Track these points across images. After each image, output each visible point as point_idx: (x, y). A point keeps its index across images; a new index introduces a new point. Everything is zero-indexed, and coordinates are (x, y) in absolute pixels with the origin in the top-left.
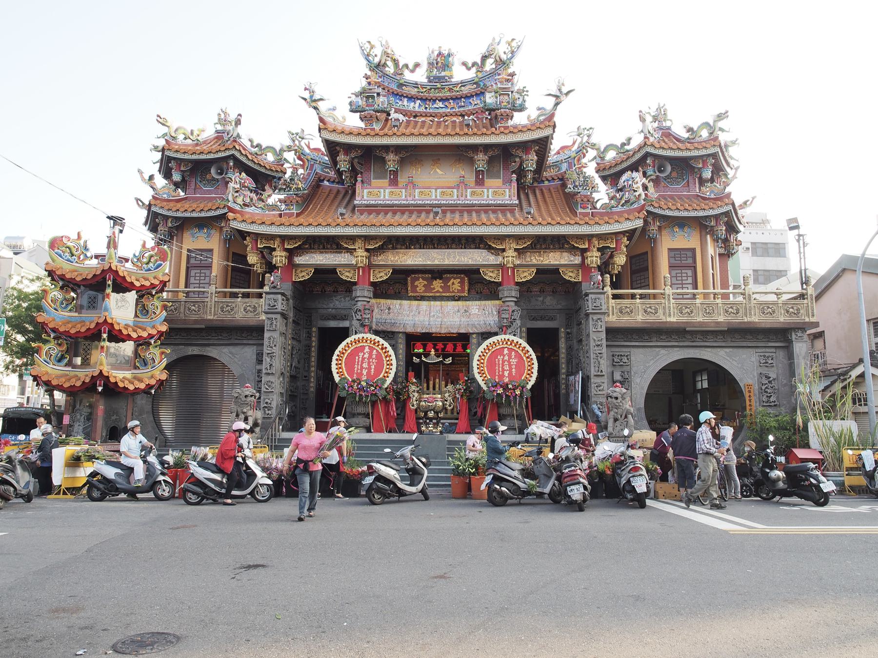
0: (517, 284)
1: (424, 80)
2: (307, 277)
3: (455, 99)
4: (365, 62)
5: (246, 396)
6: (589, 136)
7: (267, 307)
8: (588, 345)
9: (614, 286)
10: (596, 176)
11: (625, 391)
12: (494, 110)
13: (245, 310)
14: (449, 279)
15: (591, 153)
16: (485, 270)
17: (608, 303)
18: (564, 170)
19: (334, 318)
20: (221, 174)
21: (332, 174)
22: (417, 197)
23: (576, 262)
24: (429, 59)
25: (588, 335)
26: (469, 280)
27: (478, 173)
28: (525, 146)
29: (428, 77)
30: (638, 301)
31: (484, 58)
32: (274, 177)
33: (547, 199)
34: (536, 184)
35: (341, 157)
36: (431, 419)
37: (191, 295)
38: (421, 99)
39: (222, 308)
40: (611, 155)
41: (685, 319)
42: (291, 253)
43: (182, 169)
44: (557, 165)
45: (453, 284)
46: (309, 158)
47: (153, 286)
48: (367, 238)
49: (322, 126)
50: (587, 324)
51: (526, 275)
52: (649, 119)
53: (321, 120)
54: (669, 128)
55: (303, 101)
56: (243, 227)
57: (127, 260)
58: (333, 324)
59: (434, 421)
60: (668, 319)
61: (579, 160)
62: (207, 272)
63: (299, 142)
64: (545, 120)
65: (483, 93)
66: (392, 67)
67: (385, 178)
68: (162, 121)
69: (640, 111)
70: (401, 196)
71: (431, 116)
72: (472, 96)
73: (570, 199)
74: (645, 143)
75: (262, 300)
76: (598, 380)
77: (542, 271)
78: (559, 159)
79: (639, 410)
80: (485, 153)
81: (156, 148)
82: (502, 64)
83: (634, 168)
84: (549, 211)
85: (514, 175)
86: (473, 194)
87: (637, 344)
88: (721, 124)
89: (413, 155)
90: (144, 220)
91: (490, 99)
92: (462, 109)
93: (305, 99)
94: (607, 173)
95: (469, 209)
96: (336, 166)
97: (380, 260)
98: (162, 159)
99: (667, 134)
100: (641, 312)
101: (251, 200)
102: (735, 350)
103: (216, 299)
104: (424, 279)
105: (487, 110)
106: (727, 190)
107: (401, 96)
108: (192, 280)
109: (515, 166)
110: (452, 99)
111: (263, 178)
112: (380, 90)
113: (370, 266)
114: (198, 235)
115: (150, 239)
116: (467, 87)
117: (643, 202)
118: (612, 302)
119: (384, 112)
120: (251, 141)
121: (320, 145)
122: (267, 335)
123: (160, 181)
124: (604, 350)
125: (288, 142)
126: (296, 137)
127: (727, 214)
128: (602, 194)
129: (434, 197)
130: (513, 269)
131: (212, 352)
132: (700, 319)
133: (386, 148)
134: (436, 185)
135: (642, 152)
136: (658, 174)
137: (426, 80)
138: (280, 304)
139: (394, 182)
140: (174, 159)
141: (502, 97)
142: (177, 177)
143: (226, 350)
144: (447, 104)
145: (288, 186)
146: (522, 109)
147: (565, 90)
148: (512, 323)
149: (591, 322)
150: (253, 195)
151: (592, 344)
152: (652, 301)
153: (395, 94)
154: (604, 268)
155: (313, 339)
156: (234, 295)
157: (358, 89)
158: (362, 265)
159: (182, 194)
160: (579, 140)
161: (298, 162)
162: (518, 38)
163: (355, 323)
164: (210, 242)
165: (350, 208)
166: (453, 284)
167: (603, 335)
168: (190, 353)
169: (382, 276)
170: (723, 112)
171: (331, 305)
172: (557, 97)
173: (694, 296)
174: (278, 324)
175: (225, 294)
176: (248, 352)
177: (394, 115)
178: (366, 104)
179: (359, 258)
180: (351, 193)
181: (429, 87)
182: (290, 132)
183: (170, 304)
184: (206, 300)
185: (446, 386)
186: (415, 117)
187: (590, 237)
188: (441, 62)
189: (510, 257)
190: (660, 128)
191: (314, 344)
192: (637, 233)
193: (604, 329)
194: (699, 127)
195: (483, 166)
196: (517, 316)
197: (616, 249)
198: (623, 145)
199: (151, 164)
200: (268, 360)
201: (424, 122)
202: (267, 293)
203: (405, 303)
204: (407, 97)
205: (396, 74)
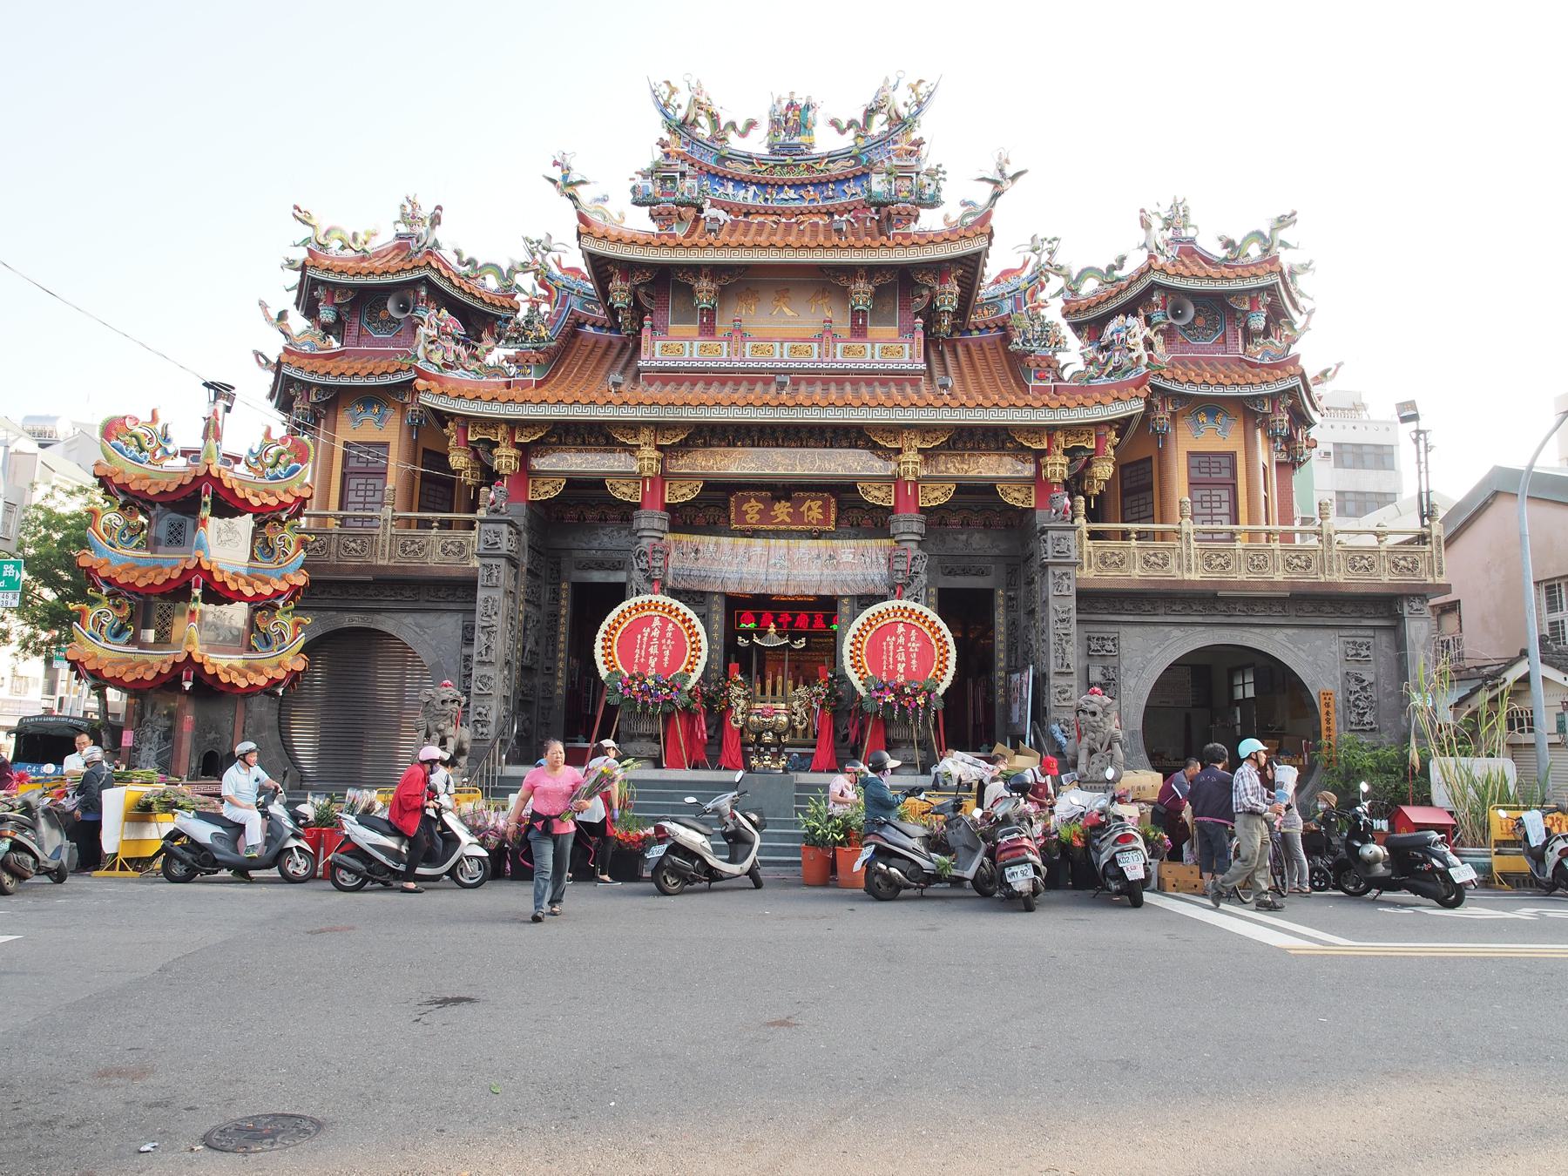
0: (922, 510)
1: (763, 150)
2: (553, 494)
4: (661, 118)
5: (443, 702)
6: (1051, 253)
7: (482, 545)
8: (1045, 619)
9: (1092, 516)
10: (1063, 323)
12: (885, 205)
13: (443, 549)
14: (804, 500)
15: (1055, 283)
17: (1081, 546)
19: (601, 566)
20: (405, 310)
21: (600, 313)
22: (748, 356)
23: (1027, 474)
25: (1046, 602)
26: (838, 502)
27: (855, 314)
28: (939, 269)
29: (771, 146)
30: (1134, 543)
31: (870, 113)
32: (498, 318)
35: (616, 284)
36: (768, 746)
37: (350, 522)
38: (758, 184)
39: (404, 546)
40: (1089, 287)
41: (1215, 576)
42: (526, 451)
43: (337, 300)
44: (994, 302)
45: (810, 508)
46: (560, 284)
47: (283, 506)
48: (660, 427)
51: (937, 496)
52: (1157, 224)
53: (582, 218)
54: (1192, 241)
56: (442, 404)
57: (237, 460)
58: (598, 577)
60: (1187, 577)
61: (1033, 295)
62: (379, 483)
63: (543, 256)
64: (974, 223)
65: (866, 175)
66: (708, 127)
69: (1142, 211)
70: (721, 354)
72: (847, 180)
76: (1063, 682)
77: (966, 489)
81: (291, 264)
82: (900, 124)
83: (1129, 309)
86: (846, 351)
88: (1283, 235)
89: (741, 281)
91: (878, 185)
92: (829, 203)
93: (554, 182)
95: (839, 377)
96: (606, 300)
97: (682, 465)
99: (1189, 250)
101: (458, 356)
102: (1304, 631)
103: (394, 531)
105: (873, 204)
106: (1293, 350)
107: (723, 178)
108: (352, 497)
109: (920, 303)
110: (812, 184)
111: (478, 319)
112: (685, 168)
113: (664, 477)
116: (839, 164)
117: (1144, 370)
119: (690, 204)
120: (458, 253)
121: (576, 260)
122: (481, 594)
123: (298, 323)
124: (1073, 629)
125: (522, 256)
126: (539, 247)
127: (1292, 392)
128: (1073, 355)
129: (777, 357)
130: (915, 484)
131: (386, 623)
133: (696, 269)
134: (782, 334)
136: (1171, 320)
137: (767, 151)
138: (505, 541)
139: (708, 329)
140: (323, 283)
141: (899, 182)
142: (327, 315)
144: (802, 192)
146: (934, 203)
147: (1010, 172)
150: (461, 349)
151: (1052, 617)
152: (1158, 544)
153: (713, 176)
154: (1075, 485)
155: (563, 602)
156: (425, 524)
157: (647, 165)
159: (336, 345)
160: (1034, 259)
163: (637, 576)
164: (385, 430)
165: (631, 373)
166: (810, 508)
167: (1072, 603)
168: (346, 625)
169: (684, 493)
170: (1288, 213)
171: (595, 544)
172: (996, 183)
173: (1232, 536)
175: (408, 522)
176: (450, 625)
177: (709, 212)
178: (660, 191)
182: (526, 239)
184: (376, 531)
185: (795, 688)
186: (747, 214)
187: (1050, 430)
189: (911, 463)
191: (563, 612)
192: (1134, 425)
193: (1073, 591)
194: (1245, 240)
195: (865, 304)
196: (921, 566)
197: (1096, 451)
198: (1112, 268)
199: (282, 291)
201: (761, 224)
202: (482, 521)
203: (725, 541)
204: (732, 179)
205: (713, 138)
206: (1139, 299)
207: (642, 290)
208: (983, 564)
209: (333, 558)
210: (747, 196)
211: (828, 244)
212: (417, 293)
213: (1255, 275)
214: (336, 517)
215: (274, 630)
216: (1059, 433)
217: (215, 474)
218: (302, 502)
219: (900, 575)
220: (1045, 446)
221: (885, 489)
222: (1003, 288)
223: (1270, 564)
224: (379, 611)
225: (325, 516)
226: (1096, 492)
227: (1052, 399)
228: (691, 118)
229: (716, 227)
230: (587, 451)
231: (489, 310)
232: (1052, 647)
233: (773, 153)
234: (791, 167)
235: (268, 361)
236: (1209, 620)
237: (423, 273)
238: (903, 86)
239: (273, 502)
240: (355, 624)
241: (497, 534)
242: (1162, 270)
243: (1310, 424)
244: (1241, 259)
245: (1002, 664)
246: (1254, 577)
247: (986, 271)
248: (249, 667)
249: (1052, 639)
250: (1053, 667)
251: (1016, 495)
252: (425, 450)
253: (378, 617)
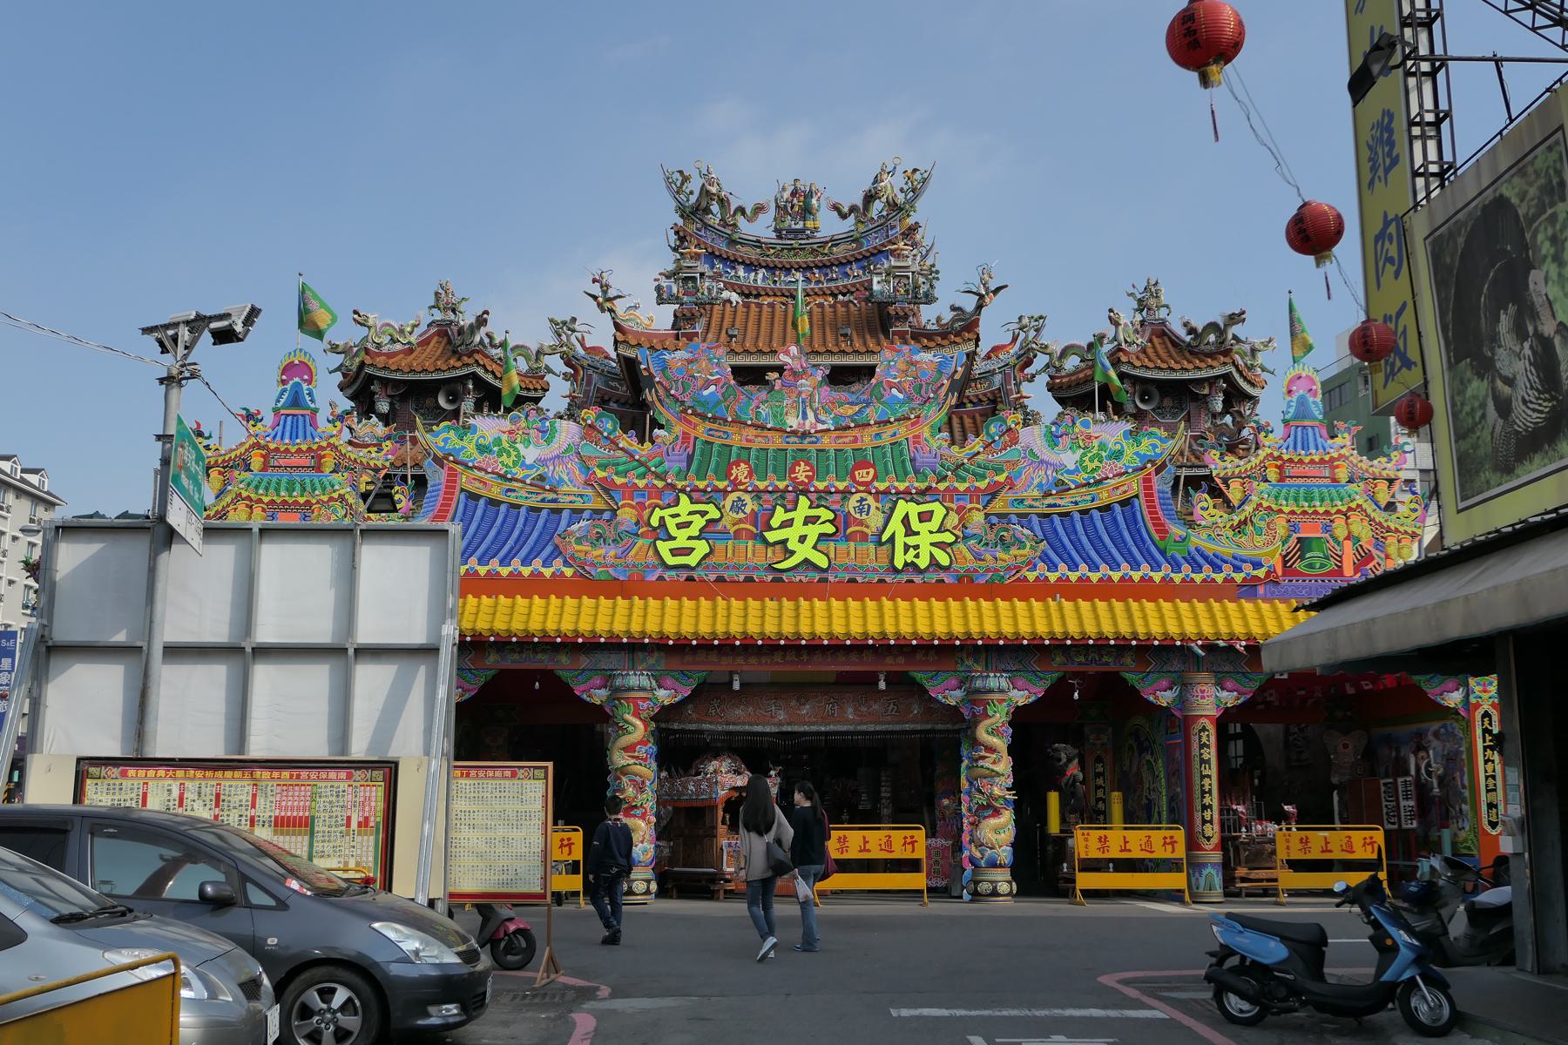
3: (822, 267)
15: (1041, 361)
29: (776, 230)
31: (870, 198)
38: (767, 267)
40: (1072, 362)
49: (620, 337)
53: (617, 326)
69: (1111, 310)
78: (989, 368)
88: (1235, 330)
92: (832, 284)
93: (595, 298)
99: (1161, 332)
107: (732, 262)
116: (842, 247)
125: (549, 340)
126: (563, 327)
146: (929, 299)
153: (724, 260)
160: (1022, 335)
182: (551, 321)
186: (758, 296)
194: (1205, 329)
204: (743, 263)
211: (835, 349)
212: (465, 385)
222: (993, 365)
228: (704, 204)
233: (780, 237)
237: (471, 370)
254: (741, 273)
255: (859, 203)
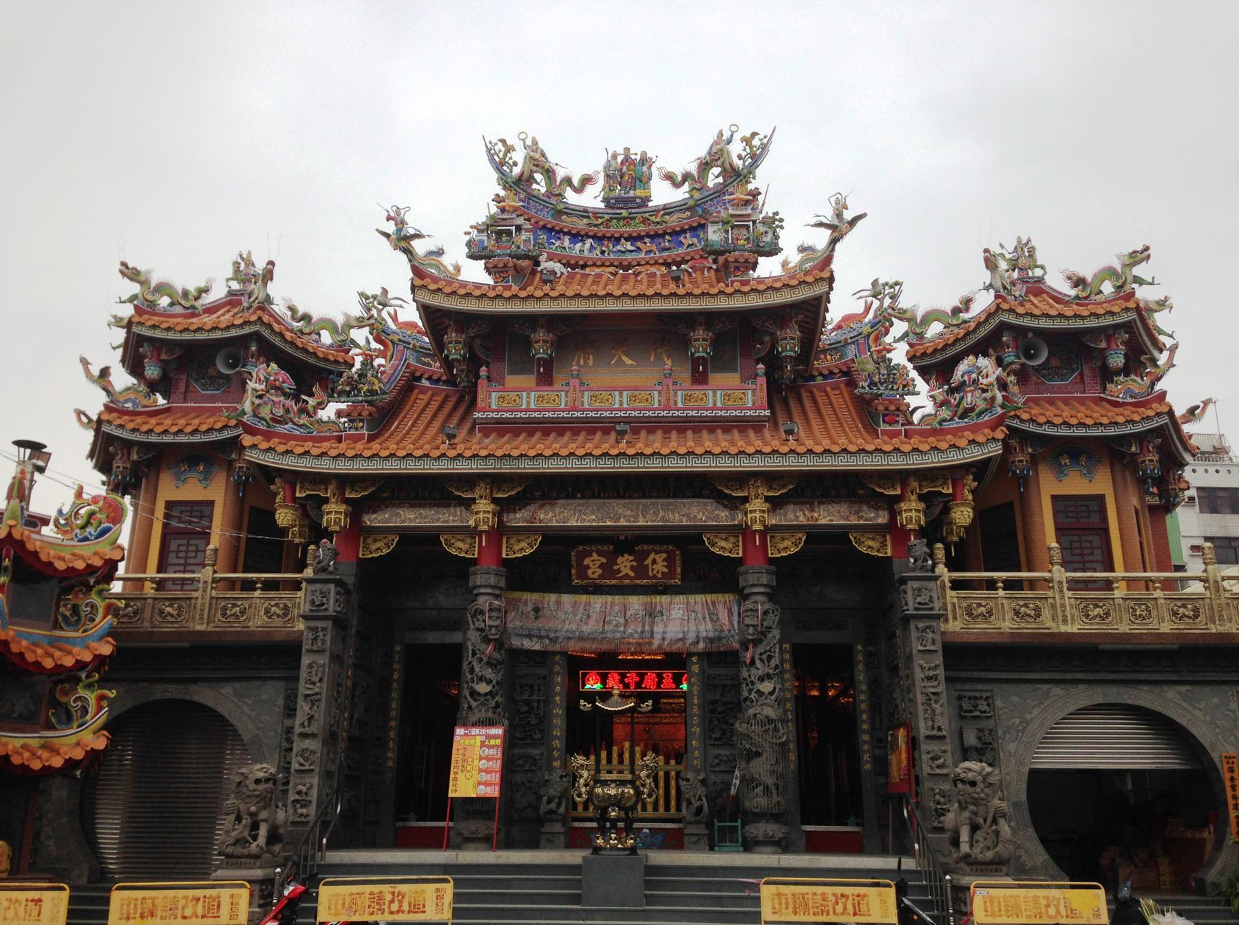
0: (772, 561)
1: (599, 204)
2: (385, 551)
3: (654, 237)
4: (495, 175)
5: (258, 781)
6: (894, 297)
7: (308, 607)
8: (910, 676)
9: (952, 565)
10: (910, 366)
11: (989, 769)
12: (722, 253)
13: (267, 612)
14: (648, 554)
15: (899, 328)
16: (711, 536)
17: (944, 597)
18: (850, 356)
19: (436, 626)
20: (233, 366)
21: (436, 366)
22: (589, 405)
23: (880, 521)
24: (607, 167)
25: (909, 658)
26: (683, 555)
27: (696, 362)
28: (780, 315)
29: (605, 200)
30: (1001, 593)
31: (705, 166)
32: (331, 372)
33: (823, 410)
34: (800, 382)
35: (452, 336)
36: (614, 822)
37: (169, 585)
38: (594, 237)
39: (225, 609)
40: (935, 329)
41: (1094, 628)
42: (357, 509)
43: (164, 356)
44: (837, 348)
45: (654, 562)
46: (395, 338)
47: (91, 569)
48: (495, 480)
49: (418, 282)
50: (906, 636)
51: (787, 547)
52: (1003, 265)
53: (417, 271)
54: (1040, 280)
55: (384, 239)
56: (269, 460)
57: (45, 521)
58: (432, 637)
59: (621, 825)
60: (1064, 629)
61: (877, 339)
62: (201, 543)
63: (379, 311)
64: (813, 268)
65: (702, 227)
66: (543, 183)
67: (531, 373)
68: (129, 273)
70: (557, 401)
71: (612, 265)
72: (683, 231)
73: (875, 408)
74: (998, 307)
75: (299, 594)
76: (935, 747)
77: (817, 537)
79: (1016, 805)
80: (708, 328)
81: (118, 321)
82: (735, 176)
83: (979, 349)
84: (826, 428)
85: (761, 366)
86: (687, 398)
87: (1005, 676)
88: (1137, 271)
89: (582, 334)
90: (88, 448)
91: (714, 234)
92: (666, 254)
93: (387, 235)
94: (929, 361)
95: (682, 426)
96: (442, 352)
97: (518, 519)
98: (127, 339)
99: (1037, 288)
100: (1009, 615)
101: (287, 411)
102: (1197, 689)
103: (214, 593)
104: (600, 554)
105: (710, 253)
106: (1159, 386)
107: (558, 232)
108: (172, 559)
109: (761, 349)
110: (648, 236)
111: (310, 371)
112: (520, 221)
113: (499, 533)
114: (188, 475)
115: (95, 484)
117: (1000, 411)
118: (951, 594)
119: (526, 257)
120: (292, 309)
121: (410, 314)
122: (305, 660)
123: (122, 379)
124: (942, 688)
125: (357, 311)
126: (376, 302)
127: (1160, 431)
128: (922, 400)
129: (617, 406)
130: (763, 534)
131: (204, 695)
132: (1124, 628)
133: (533, 320)
134: (621, 386)
135: (994, 322)
136: (1023, 360)
137: (602, 205)
138: (332, 603)
139: (546, 379)
140: (151, 340)
141: (736, 231)
142: (152, 372)
143: (227, 689)
144: (639, 244)
145: (354, 385)
146: (773, 251)
147: (848, 215)
148: (764, 634)
149: (914, 634)
150: (290, 403)
151: (919, 675)
152: (1029, 594)
153: (549, 230)
154: (933, 530)
155: (396, 666)
156: (249, 585)
157: (482, 218)
158: (485, 528)
159: (161, 401)
160: (876, 304)
161: (374, 345)
162: (764, 131)
163: (473, 636)
164: (215, 491)
165: (467, 426)
166: (654, 562)
167: (939, 659)
168: (157, 697)
169: (523, 548)
170: (1139, 248)
171: (430, 603)
172: (832, 227)
173: (1108, 585)
174: (328, 638)
175: (231, 584)
176: (272, 692)
177: (546, 265)
178: (491, 241)
179: (481, 515)
180: (468, 399)
181: (607, 217)
182: (362, 295)
183: (122, 604)
184: (195, 594)
185: (644, 755)
186: (584, 267)
187: (902, 477)
188: (629, 174)
189: (757, 511)
190: (1024, 281)
191: (396, 676)
192: (993, 468)
193: (938, 647)
195: (705, 350)
196: (772, 620)
197: (953, 496)
198: (956, 311)
199: (107, 349)
200: (306, 708)
201: (599, 276)
202: (309, 581)
203: (567, 599)
204: (569, 233)
205: (550, 194)
206: (991, 337)
207: (478, 342)
208: (837, 602)
209: (146, 624)
210: (583, 249)
212: (247, 348)
213: (953, 446)
214: (152, 580)
215: (74, 706)
216: (912, 478)
217: (17, 536)
218: (112, 565)
219: (751, 630)
220: (899, 492)
221: (732, 539)
223: (1154, 613)
224: (195, 681)
225: (142, 580)
226: (955, 539)
227: (902, 443)
229: (552, 278)
230: (422, 506)
231: (323, 365)
232: (920, 708)
234: (628, 220)
235: (90, 420)
236: (1090, 676)
238: (737, 137)
239: (80, 565)
240: (168, 696)
241: (324, 595)
242: (1011, 310)
243: (1182, 465)
244: (1093, 297)
245: (865, 727)
246: (1138, 629)
247: (828, 316)
248: (44, 747)
249: (920, 699)
250: (923, 730)
251: (871, 543)
252: (252, 508)
253: (193, 687)
254: (567, 243)
255: (693, 168)
